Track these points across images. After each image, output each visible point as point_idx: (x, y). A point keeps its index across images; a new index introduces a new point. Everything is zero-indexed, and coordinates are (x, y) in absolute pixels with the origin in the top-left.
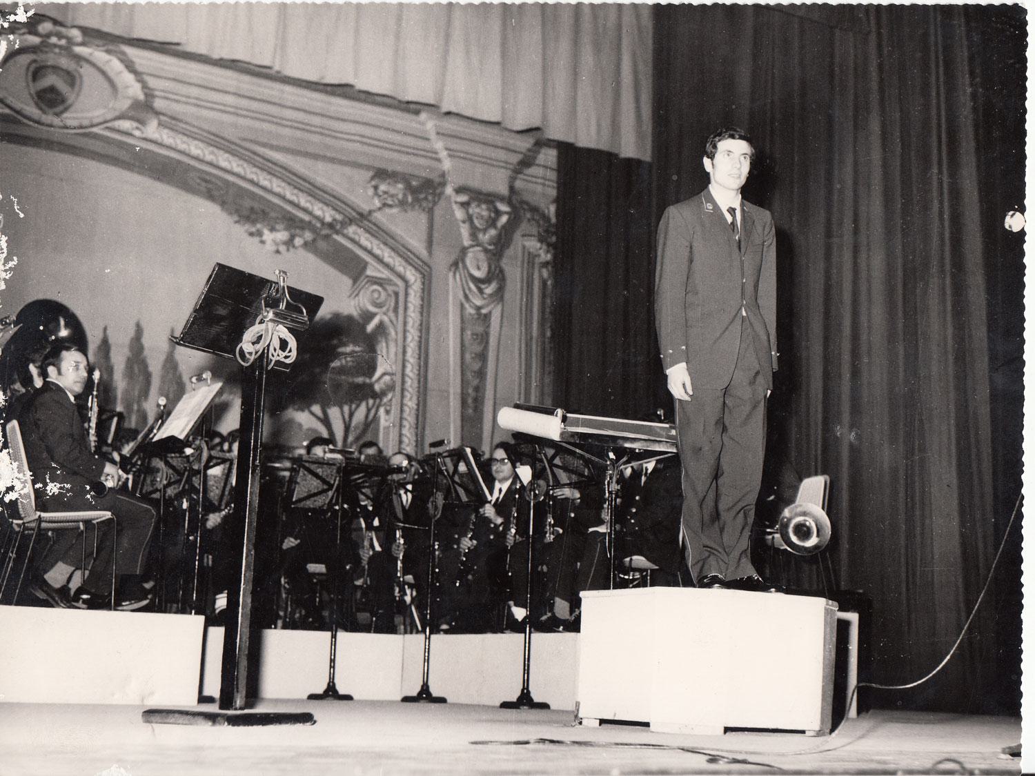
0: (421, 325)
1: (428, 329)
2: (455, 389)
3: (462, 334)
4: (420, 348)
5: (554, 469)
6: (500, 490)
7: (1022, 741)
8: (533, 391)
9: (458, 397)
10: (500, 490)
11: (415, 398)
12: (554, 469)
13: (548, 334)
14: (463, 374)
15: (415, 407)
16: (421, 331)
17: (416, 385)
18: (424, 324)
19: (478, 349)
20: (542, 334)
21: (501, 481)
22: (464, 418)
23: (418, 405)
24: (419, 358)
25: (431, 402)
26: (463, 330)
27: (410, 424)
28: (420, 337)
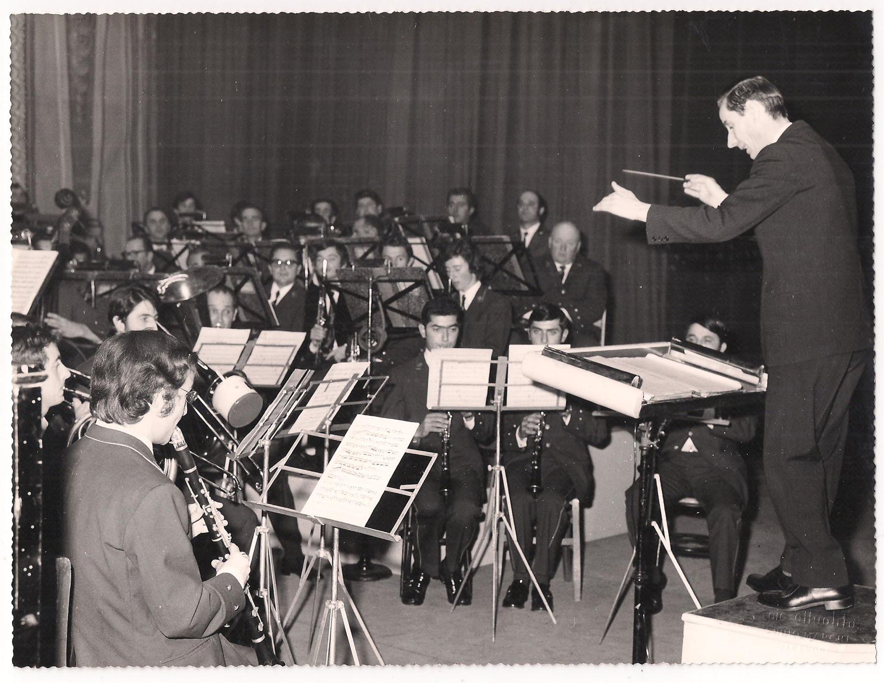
0: (25, 25)
1: (33, 33)
2: (62, 95)
3: (68, 38)
4: (25, 52)
5: (388, 311)
6: (278, 294)
7: (11, 357)
8: (140, 97)
9: (66, 105)
10: (278, 294)
11: (22, 106)
12: (388, 311)
13: (154, 36)
14: (70, 80)
15: (23, 116)
16: (25, 32)
17: (22, 92)
18: (28, 25)
19: (84, 53)
20: (148, 36)
21: (280, 284)
22: (73, 125)
23: (26, 114)
24: (25, 63)
25: (40, 111)
26: (68, 32)
27: (19, 133)
28: (25, 39)
